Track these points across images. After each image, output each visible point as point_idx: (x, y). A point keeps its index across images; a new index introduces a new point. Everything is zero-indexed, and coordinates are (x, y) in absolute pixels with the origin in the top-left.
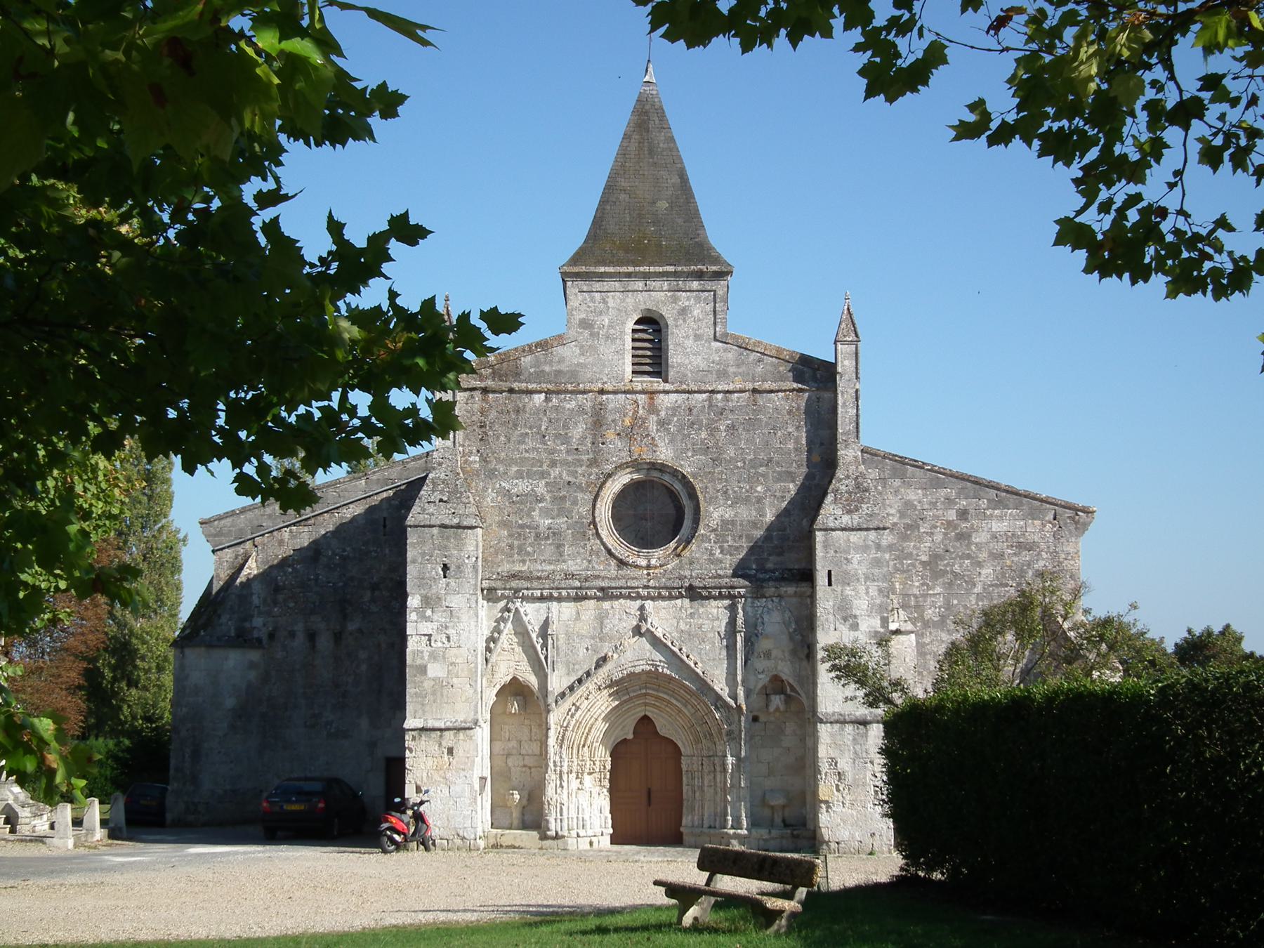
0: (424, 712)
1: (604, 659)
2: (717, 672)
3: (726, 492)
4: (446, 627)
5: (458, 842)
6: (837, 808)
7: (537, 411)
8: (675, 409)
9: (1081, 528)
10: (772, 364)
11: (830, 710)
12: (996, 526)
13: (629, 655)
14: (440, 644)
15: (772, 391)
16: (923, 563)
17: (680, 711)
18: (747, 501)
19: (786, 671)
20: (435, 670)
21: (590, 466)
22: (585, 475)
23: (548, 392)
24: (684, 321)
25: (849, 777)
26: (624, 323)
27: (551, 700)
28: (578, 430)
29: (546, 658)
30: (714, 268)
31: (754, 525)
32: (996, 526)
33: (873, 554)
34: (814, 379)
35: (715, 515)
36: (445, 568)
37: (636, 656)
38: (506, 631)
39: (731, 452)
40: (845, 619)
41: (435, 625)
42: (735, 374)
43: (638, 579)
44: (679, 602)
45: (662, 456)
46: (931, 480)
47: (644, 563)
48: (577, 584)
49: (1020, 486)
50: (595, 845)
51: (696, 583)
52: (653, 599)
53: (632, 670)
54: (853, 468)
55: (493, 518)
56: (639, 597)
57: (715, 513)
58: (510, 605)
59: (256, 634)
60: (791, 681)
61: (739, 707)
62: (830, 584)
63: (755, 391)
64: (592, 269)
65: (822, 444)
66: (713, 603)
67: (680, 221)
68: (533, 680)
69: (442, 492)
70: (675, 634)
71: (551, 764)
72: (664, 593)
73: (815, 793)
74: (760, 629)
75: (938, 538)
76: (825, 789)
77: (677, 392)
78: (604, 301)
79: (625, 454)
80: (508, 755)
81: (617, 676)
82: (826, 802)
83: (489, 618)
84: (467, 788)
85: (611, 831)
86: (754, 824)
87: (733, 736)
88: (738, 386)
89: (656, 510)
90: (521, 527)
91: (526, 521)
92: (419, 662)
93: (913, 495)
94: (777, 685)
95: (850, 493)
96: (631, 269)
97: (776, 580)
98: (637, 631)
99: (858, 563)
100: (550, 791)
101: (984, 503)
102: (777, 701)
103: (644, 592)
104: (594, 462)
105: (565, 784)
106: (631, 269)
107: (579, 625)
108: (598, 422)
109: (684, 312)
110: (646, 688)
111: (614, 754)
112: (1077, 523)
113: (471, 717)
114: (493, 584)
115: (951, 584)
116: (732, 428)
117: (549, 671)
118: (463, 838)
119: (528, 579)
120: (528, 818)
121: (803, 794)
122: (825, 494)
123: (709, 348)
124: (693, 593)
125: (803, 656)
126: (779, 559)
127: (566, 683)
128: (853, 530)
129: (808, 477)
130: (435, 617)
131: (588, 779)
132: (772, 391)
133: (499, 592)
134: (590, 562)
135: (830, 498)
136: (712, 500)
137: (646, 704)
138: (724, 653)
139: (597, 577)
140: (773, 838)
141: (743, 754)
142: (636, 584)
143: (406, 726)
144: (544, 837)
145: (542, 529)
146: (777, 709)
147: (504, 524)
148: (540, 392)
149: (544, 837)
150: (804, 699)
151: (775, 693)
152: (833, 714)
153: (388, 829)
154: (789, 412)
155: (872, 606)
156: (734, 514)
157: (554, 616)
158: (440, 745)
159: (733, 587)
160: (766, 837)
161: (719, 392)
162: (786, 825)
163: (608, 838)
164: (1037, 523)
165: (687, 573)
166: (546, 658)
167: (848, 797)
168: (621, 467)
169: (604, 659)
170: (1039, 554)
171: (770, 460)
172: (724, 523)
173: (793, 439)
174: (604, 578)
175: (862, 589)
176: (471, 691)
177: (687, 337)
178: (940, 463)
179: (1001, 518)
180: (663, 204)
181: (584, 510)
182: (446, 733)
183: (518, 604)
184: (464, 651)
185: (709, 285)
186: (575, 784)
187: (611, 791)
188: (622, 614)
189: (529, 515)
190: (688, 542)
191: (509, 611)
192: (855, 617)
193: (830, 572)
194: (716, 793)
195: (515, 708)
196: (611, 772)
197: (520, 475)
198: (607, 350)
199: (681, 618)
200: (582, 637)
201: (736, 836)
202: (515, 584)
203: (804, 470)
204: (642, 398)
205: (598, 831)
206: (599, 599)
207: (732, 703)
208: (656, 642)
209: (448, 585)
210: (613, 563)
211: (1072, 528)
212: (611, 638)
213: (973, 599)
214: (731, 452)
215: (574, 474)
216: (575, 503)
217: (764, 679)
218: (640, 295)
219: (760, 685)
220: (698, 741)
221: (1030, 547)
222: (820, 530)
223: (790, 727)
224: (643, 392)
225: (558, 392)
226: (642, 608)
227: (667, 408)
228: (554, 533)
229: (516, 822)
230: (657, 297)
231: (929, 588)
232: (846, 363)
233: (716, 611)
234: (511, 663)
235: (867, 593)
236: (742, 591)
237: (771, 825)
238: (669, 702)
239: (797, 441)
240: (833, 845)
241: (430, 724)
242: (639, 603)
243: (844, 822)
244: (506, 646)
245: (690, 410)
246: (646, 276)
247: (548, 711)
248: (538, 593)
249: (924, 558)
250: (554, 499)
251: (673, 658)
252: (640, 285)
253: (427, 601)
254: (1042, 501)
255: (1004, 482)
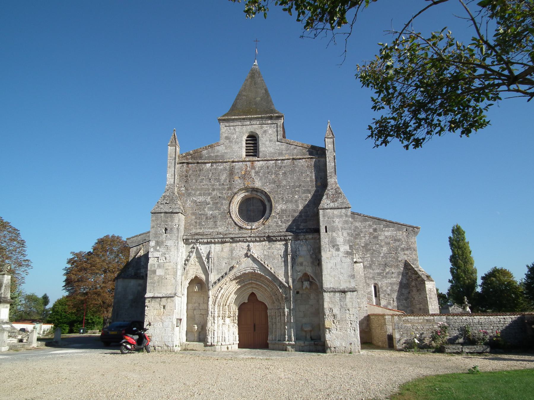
0: (154, 290)
1: (233, 267)
2: (280, 272)
3: (282, 199)
4: (165, 254)
5: (166, 348)
6: (334, 331)
7: (208, 170)
8: (262, 167)
9: (416, 233)
10: (300, 149)
11: (329, 286)
12: (387, 234)
13: (243, 265)
14: (162, 261)
15: (300, 159)
16: (363, 247)
17: (266, 290)
18: (291, 202)
19: (309, 271)
20: (159, 272)
21: (228, 190)
22: (226, 194)
23: (212, 163)
24: (265, 135)
25: (339, 317)
26: (242, 137)
27: (210, 285)
28: (223, 177)
29: (209, 267)
30: (276, 115)
31: (295, 211)
32: (387, 234)
33: (344, 218)
34: (317, 154)
35: (279, 208)
36: (166, 229)
37: (246, 266)
38: (192, 257)
39: (284, 183)
40: (334, 246)
41: (160, 253)
42: (286, 154)
43: (246, 234)
44: (264, 243)
45: (257, 185)
46: (364, 219)
47: (249, 227)
48: (222, 236)
49: (394, 221)
50: (230, 349)
51: (271, 235)
52: (253, 242)
53: (244, 272)
54: (334, 186)
55: (189, 212)
56: (247, 241)
57: (278, 207)
58: (195, 246)
59: (142, 275)
60: (312, 275)
61: (290, 287)
62: (326, 232)
63: (293, 159)
64: (230, 117)
65: (321, 178)
66: (278, 243)
67: (265, 103)
68: (203, 277)
69: (167, 200)
70: (262, 256)
71: (210, 313)
72: (258, 239)
73: (324, 325)
74: (298, 253)
75: (367, 238)
76: (328, 323)
77: (262, 160)
78: (235, 129)
79: (242, 185)
80: (195, 309)
81: (238, 274)
82: (329, 329)
83: (186, 251)
84: (170, 324)
85: (238, 342)
86: (297, 339)
87: (287, 300)
88: (287, 157)
89: (256, 207)
90: (200, 215)
91: (202, 212)
92: (153, 269)
93: (358, 224)
94: (306, 277)
95: (333, 195)
96: (244, 117)
97: (304, 232)
98: (246, 255)
99: (338, 222)
100: (209, 325)
101: (382, 226)
102: (306, 284)
103: (249, 239)
104: (230, 189)
105: (216, 322)
106: (244, 117)
107: (223, 253)
108: (231, 173)
109: (265, 132)
110: (251, 280)
111: (239, 309)
112: (414, 232)
113: (174, 292)
114: (188, 237)
115: (372, 253)
116: (285, 173)
117: (210, 273)
118: (168, 346)
119: (202, 235)
120: (202, 337)
121: (319, 325)
122: (323, 196)
123: (275, 144)
124: (270, 239)
125: (316, 264)
126: (305, 224)
127: (217, 278)
128: (335, 209)
129: (316, 191)
130: (161, 250)
131: (228, 320)
132: (300, 159)
133: (190, 241)
134: (227, 228)
135: (325, 197)
136: (277, 202)
137: (252, 287)
138: (283, 264)
139: (230, 234)
140: (306, 346)
141: (292, 307)
142: (246, 235)
143: (146, 296)
144: (206, 346)
145: (208, 215)
146: (306, 288)
147: (193, 214)
148: (209, 163)
149: (206, 346)
150: (318, 283)
151: (306, 281)
152: (330, 288)
153: (124, 342)
154: (308, 167)
155: (345, 241)
156: (286, 207)
157: (212, 250)
158: (160, 304)
159: (286, 236)
160: (303, 345)
161: (279, 160)
162: (312, 339)
163: (237, 345)
164: (401, 232)
165: (267, 231)
166: (209, 267)
167: (338, 326)
168: (241, 190)
169: (233, 267)
170: (402, 243)
171: (300, 185)
172: (282, 211)
173: (310, 176)
174: (232, 234)
175: (340, 233)
176: (174, 281)
177: (267, 141)
178: (366, 214)
179: (388, 231)
180: (258, 99)
181: (225, 207)
182: (163, 299)
183: (198, 245)
184: (172, 264)
185: (275, 122)
186: (221, 322)
187: (239, 325)
188: (240, 248)
189: (204, 210)
190: (268, 219)
191: (194, 248)
192: (338, 245)
193: (326, 227)
194: (281, 325)
195: (196, 289)
196: (239, 316)
197: (200, 195)
198: (235, 147)
199: (265, 249)
200: (224, 258)
201: (289, 345)
202: (196, 237)
203: (314, 189)
204: (249, 164)
205: (231, 342)
206: (231, 242)
207: (287, 285)
208: (254, 260)
209: (166, 236)
210: (237, 228)
211: (413, 233)
212: (236, 259)
213: (380, 258)
214: (284, 183)
215: (222, 193)
216: (222, 204)
217: (300, 275)
218: (248, 127)
219: (298, 278)
220: (274, 303)
221: (399, 240)
222: (321, 209)
223: (312, 296)
224: (249, 161)
225: (216, 163)
226: (248, 246)
227: (259, 167)
228: (213, 217)
229: (196, 339)
230: (255, 127)
231: (365, 255)
232: (329, 146)
233: (279, 246)
234: (195, 270)
235: (343, 235)
236: (290, 237)
237: (306, 339)
238: (261, 286)
239: (311, 177)
240: (333, 349)
241: (156, 295)
242: (247, 243)
243: (337, 338)
244: (193, 263)
245: (268, 167)
246: (250, 119)
247: (209, 290)
248: (206, 241)
249: (363, 245)
250: (214, 203)
251: (262, 266)
252: (248, 123)
253: (158, 243)
254: (401, 225)
255: (388, 220)
